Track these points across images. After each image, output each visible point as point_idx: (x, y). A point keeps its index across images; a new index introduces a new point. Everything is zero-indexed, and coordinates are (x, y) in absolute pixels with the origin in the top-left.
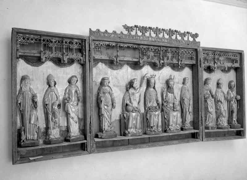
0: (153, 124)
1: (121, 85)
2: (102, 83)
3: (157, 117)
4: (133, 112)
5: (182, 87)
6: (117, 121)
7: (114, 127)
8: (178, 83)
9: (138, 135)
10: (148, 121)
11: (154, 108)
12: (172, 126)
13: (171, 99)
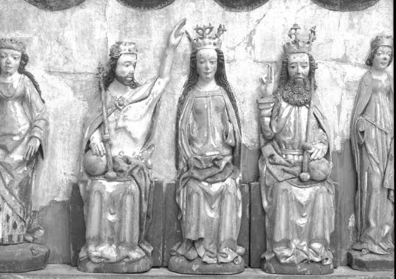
0: (198, 230)
1: (79, 68)
2: (95, 98)
3: (216, 205)
4: (110, 180)
5: (362, 79)
6: (58, 208)
7: (46, 229)
8: (344, 60)
9: (125, 269)
10: (179, 218)
11: (204, 166)
12: (288, 246)
13: (292, 129)
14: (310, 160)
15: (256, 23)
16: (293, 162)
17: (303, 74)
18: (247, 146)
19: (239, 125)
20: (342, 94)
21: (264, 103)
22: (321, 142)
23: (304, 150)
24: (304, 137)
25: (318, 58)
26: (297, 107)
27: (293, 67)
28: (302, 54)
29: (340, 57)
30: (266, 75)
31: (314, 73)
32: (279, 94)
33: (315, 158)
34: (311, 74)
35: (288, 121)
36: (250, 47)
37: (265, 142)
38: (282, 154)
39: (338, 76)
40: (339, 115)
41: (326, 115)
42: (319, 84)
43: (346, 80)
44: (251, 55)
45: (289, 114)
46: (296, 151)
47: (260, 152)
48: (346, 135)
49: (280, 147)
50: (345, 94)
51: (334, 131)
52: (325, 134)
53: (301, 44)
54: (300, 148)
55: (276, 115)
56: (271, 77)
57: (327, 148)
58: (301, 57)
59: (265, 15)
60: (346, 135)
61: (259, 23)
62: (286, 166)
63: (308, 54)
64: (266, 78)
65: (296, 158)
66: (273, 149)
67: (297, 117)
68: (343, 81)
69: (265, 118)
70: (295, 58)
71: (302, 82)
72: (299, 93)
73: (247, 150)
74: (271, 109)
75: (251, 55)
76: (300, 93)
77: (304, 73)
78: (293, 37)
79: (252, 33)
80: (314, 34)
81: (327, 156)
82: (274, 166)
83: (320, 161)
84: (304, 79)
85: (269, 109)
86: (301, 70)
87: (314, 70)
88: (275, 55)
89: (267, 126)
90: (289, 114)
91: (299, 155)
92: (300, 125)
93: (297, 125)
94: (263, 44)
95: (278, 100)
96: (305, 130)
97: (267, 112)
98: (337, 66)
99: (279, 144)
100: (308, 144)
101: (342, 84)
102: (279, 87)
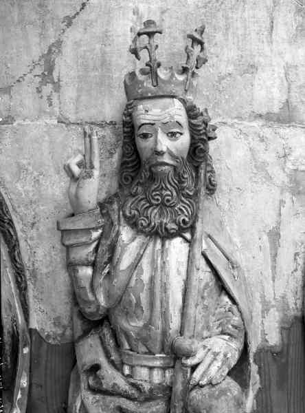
13: (144, 297)
14: (190, 387)
15: (63, 26)
16: (147, 387)
17: (171, 154)
18: (44, 335)
19: (22, 289)
20: (282, 202)
21: (76, 231)
22: (223, 333)
23: (176, 356)
24: (175, 323)
25: (220, 112)
26: (159, 241)
27: (145, 136)
28: (168, 100)
29: (276, 110)
30: (79, 158)
31: (205, 151)
32: (115, 206)
33: (203, 382)
34: (197, 153)
35: (134, 278)
36: (50, 86)
37: (85, 327)
38: (123, 364)
39: (270, 157)
40: (275, 256)
41: (238, 257)
42: (223, 179)
43: (290, 166)
44: (51, 105)
45: (139, 258)
46: (156, 358)
47: (70, 352)
48: (292, 306)
49: (118, 345)
50: (288, 201)
51: (263, 297)
52: (234, 308)
53: (162, 74)
54: (167, 349)
55: (106, 260)
56: (91, 163)
57: (241, 347)
58: (164, 108)
59: (84, 5)
60: (292, 306)
61: (69, 24)
62: (129, 398)
63: (184, 101)
64: (79, 165)
65: (157, 377)
66: (100, 349)
67: (160, 267)
68: (284, 169)
69: (78, 268)
70: (150, 112)
71: (172, 173)
72: (162, 203)
73: (45, 346)
74: (94, 245)
75: (51, 105)
76: (164, 205)
77: (173, 150)
78: (144, 54)
79: (54, 49)
80: (202, 49)
81: (239, 372)
82: (98, 397)
83: (216, 390)
84: (175, 168)
85: (87, 244)
86: (164, 143)
87: (204, 142)
88: (110, 107)
89: (84, 288)
90: (139, 258)
91: (164, 369)
92: (165, 289)
93: (156, 287)
94: (81, 79)
95: (112, 223)
96: (180, 302)
97: (86, 253)
98: (267, 132)
99: (115, 336)
100: (185, 343)
101: (281, 177)
102: (120, 186)
